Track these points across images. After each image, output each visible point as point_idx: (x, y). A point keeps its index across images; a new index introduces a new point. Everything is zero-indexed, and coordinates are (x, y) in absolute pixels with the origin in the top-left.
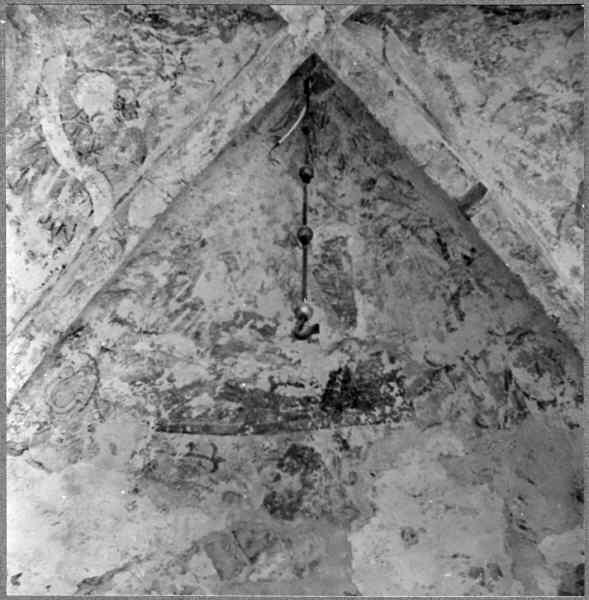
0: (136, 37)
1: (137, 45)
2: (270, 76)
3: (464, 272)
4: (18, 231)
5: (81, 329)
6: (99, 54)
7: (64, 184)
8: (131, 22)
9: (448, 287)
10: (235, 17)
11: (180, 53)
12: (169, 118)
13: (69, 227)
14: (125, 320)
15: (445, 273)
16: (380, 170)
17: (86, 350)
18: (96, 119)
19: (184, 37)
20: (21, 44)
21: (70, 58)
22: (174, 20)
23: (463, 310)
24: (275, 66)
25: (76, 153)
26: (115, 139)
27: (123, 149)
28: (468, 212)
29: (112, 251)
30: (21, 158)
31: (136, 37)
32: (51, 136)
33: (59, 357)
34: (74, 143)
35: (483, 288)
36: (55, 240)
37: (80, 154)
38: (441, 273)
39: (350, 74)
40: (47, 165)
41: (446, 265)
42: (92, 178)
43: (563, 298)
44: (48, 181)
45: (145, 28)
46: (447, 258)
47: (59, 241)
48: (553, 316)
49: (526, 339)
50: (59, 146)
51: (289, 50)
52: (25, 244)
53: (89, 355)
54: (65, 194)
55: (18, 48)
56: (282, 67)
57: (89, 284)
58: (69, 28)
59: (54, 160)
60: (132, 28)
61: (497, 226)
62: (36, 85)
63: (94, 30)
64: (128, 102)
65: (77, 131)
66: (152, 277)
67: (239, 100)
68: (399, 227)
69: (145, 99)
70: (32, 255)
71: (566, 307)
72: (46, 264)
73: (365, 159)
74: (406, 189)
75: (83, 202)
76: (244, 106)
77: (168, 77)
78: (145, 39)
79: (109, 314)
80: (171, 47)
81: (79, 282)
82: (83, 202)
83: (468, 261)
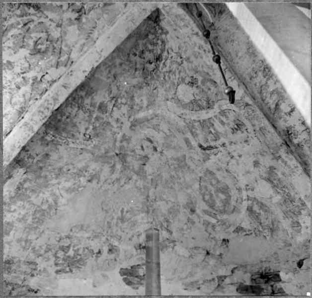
0: (164, 70)
1: (168, 70)
2: (181, 20)
4: (235, 143)
5: (288, 131)
6: (170, 87)
7: (219, 118)
8: (158, 70)
10: (157, 27)
11: (172, 53)
12: (199, 66)
13: (237, 122)
14: (292, 109)
17: (300, 132)
18: (196, 96)
19: (166, 50)
20: (160, 118)
21: (170, 100)
22: (159, 52)
25: (208, 109)
26: (205, 91)
27: (209, 89)
29: (249, 110)
30: (205, 132)
31: (164, 70)
32: (198, 117)
33: (298, 145)
34: (204, 108)
36: (243, 130)
37: (209, 108)
40: (210, 123)
42: (220, 106)
44: (217, 124)
45: (161, 65)
47: (244, 129)
50: (204, 115)
51: (170, 8)
52: (241, 143)
53: (304, 130)
54: (224, 119)
55: (161, 120)
58: (157, 97)
59: (209, 119)
60: (161, 70)
62: (177, 117)
63: (160, 86)
64: (190, 81)
65: (199, 106)
66: (274, 91)
69: (191, 74)
70: (246, 141)
72: (252, 137)
75: (229, 113)
76: (194, 34)
77: (182, 61)
78: (166, 66)
79: (285, 116)
80: (170, 57)
81: (260, 129)
82: (229, 113)
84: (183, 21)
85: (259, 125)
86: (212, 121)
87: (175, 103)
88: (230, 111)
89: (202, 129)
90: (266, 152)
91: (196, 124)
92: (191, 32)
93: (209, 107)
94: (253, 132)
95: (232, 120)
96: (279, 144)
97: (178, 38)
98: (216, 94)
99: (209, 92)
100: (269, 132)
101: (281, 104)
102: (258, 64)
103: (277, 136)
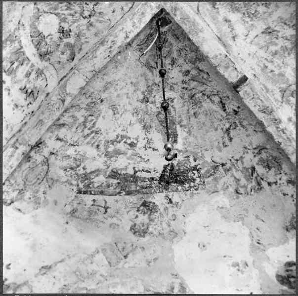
3: (233, 118)
4: (9, 94)
7: (32, 70)
9: (224, 125)
12: (86, 38)
15: (224, 118)
16: (193, 66)
17: (42, 154)
18: (49, 37)
21: (36, 6)
23: (232, 136)
24: (143, 13)
25: (38, 55)
27: (63, 53)
28: (238, 89)
30: (10, 57)
32: (26, 46)
33: (30, 157)
34: (38, 50)
35: (243, 126)
37: (41, 55)
38: (222, 118)
39: (181, 18)
40: (24, 60)
41: (224, 114)
42: (46, 67)
43: (284, 133)
46: (225, 110)
47: (30, 99)
48: (278, 142)
49: (263, 152)
53: (44, 156)
54: (33, 75)
56: (147, 14)
57: (46, 121)
61: (252, 97)
62: (18, 20)
65: (39, 43)
67: (124, 30)
68: (201, 94)
69: (74, 28)
70: (17, 106)
71: (285, 137)
73: (185, 61)
74: (205, 76)
79: (54, 136)
81: (40, 120)
83: (236, 112)
84: (138, 21)
85: (45, 118)
86: (26, 62)
87: (34, 13)
88: (45, 80)
89: (13, 53)
90: (12, 130)
91: (17, 44)
92: (128, 30)
93: (42, 56)
94: (30, 111)
95: (36, 86)
96: (30, 143)
97: (114, 12)
98: (59, 62)
99: (59, 53)
100: (40, 129)
101: (65, 128)
102: (97, 96)
103: (37, 138)
